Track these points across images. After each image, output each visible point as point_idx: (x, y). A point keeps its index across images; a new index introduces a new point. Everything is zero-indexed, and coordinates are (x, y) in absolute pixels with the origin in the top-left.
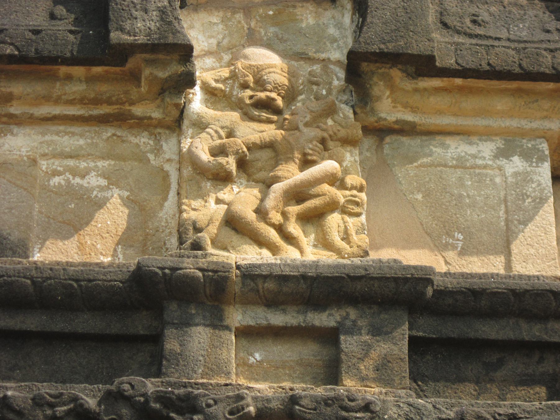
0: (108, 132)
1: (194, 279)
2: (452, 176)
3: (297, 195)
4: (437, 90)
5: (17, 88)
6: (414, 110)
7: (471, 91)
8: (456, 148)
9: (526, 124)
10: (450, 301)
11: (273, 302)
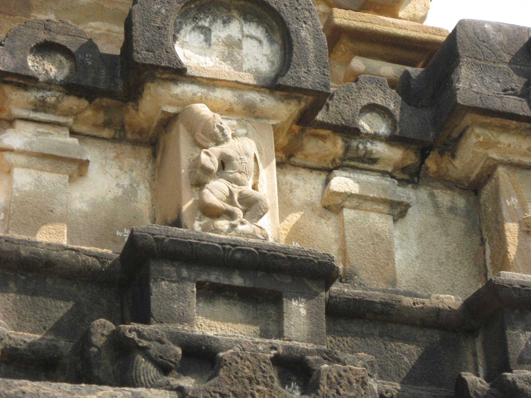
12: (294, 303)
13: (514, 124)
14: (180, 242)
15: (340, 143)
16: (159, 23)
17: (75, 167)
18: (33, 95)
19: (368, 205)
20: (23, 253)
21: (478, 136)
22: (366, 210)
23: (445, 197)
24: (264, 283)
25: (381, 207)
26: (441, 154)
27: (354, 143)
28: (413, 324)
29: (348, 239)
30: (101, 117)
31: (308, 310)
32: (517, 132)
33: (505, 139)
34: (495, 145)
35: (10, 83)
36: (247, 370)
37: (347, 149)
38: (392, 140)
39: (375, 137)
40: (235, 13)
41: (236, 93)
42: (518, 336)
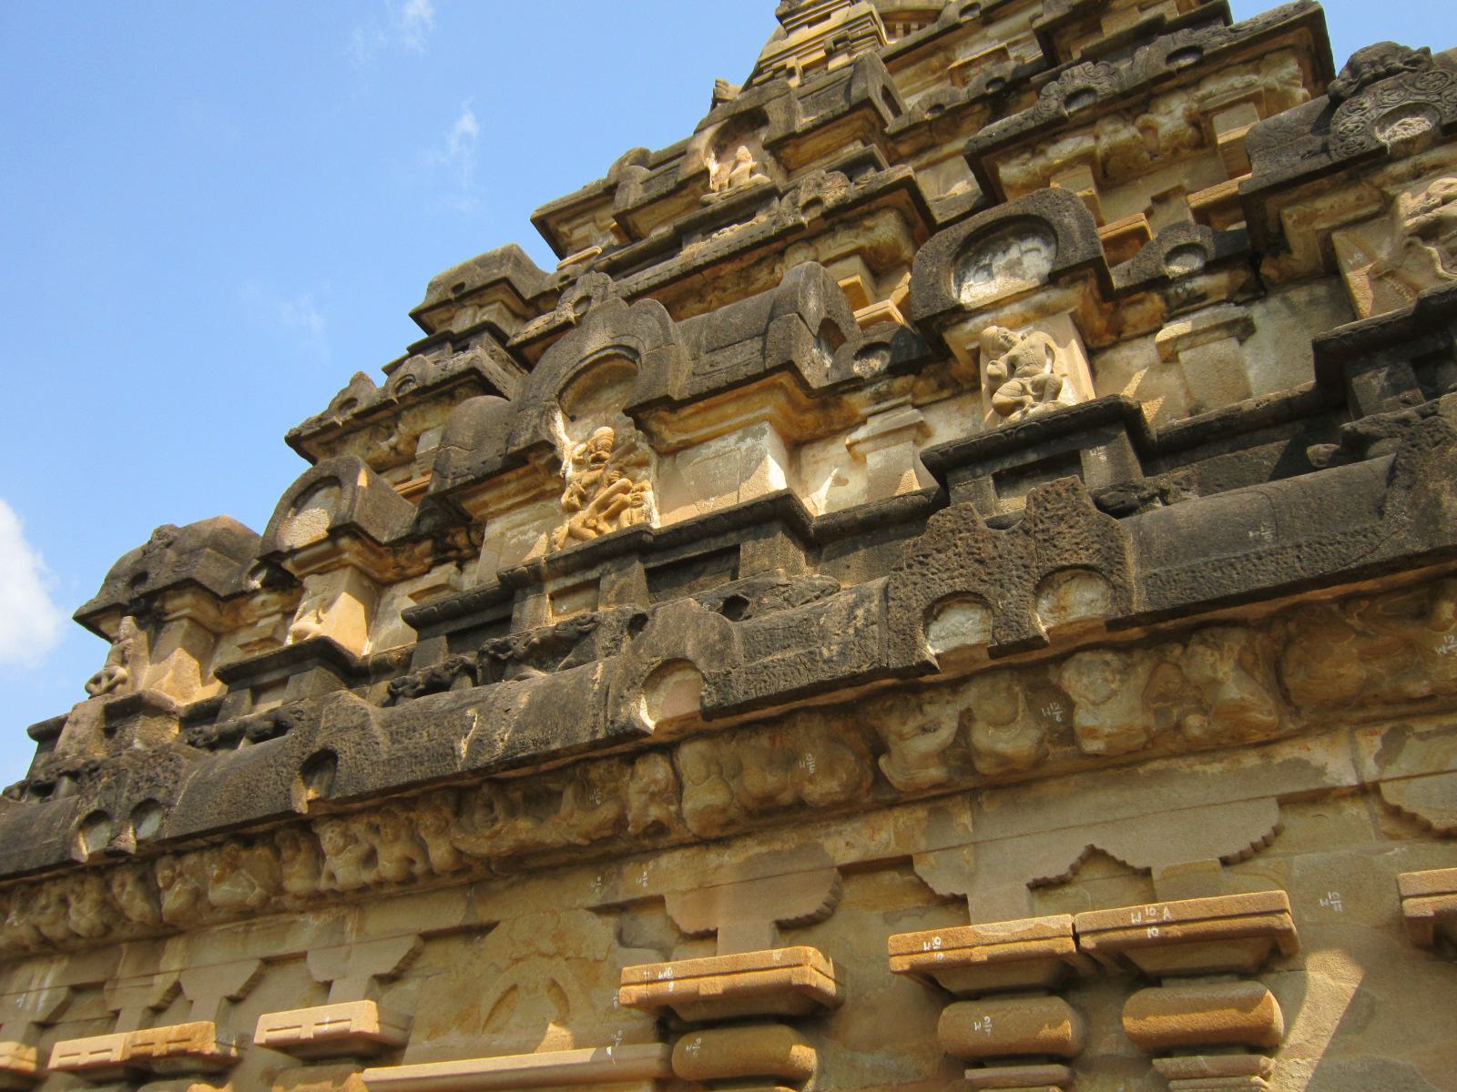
0: (539, 505)
1: (523, 573)
2: (712, 464)
3: (603, 505)
4: (691, 415)
5: (487, 497)
6: (686, 432)
7: (710, 408)
8: (716, 445)
9: (751, 416)
10: (665, 540)
11: (567, 573)
12: (1092, 454)
13: (1324, 182)
14: (964, 447)
15: (1156, 297)
16: (931, 280)
17: (914, 432)
18: (868, 392)
19: (1202, 338)
20: (859, 516)
21: (1291, 216)
22: (1203, 344)
23: (1299, 296)
24: (1058, 448)
25: (1217, 334)
26: (1275, 255)
27: (1171, 291)
28: (1268, 427)
29: (1189, 378)
30: (933, 382)
31: (1109, 455)
32: (1335, 188)
33: (1322, 204)
34: (1314, 216)
35: (844, 392)
36: (948, 524)
37: (1166, 300)
38: (1209, 268)
39: (1190, 276)
40: (1011, 240)
41: (1023, 302)
42: (1368, 383)
